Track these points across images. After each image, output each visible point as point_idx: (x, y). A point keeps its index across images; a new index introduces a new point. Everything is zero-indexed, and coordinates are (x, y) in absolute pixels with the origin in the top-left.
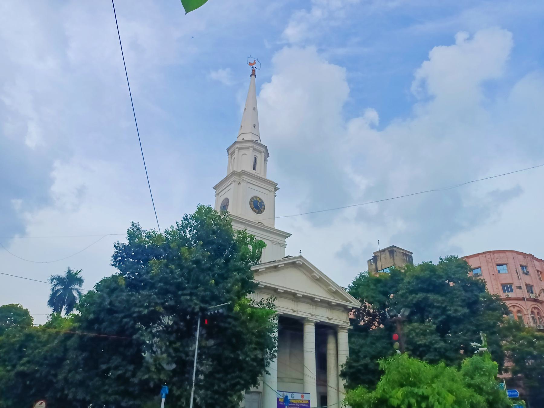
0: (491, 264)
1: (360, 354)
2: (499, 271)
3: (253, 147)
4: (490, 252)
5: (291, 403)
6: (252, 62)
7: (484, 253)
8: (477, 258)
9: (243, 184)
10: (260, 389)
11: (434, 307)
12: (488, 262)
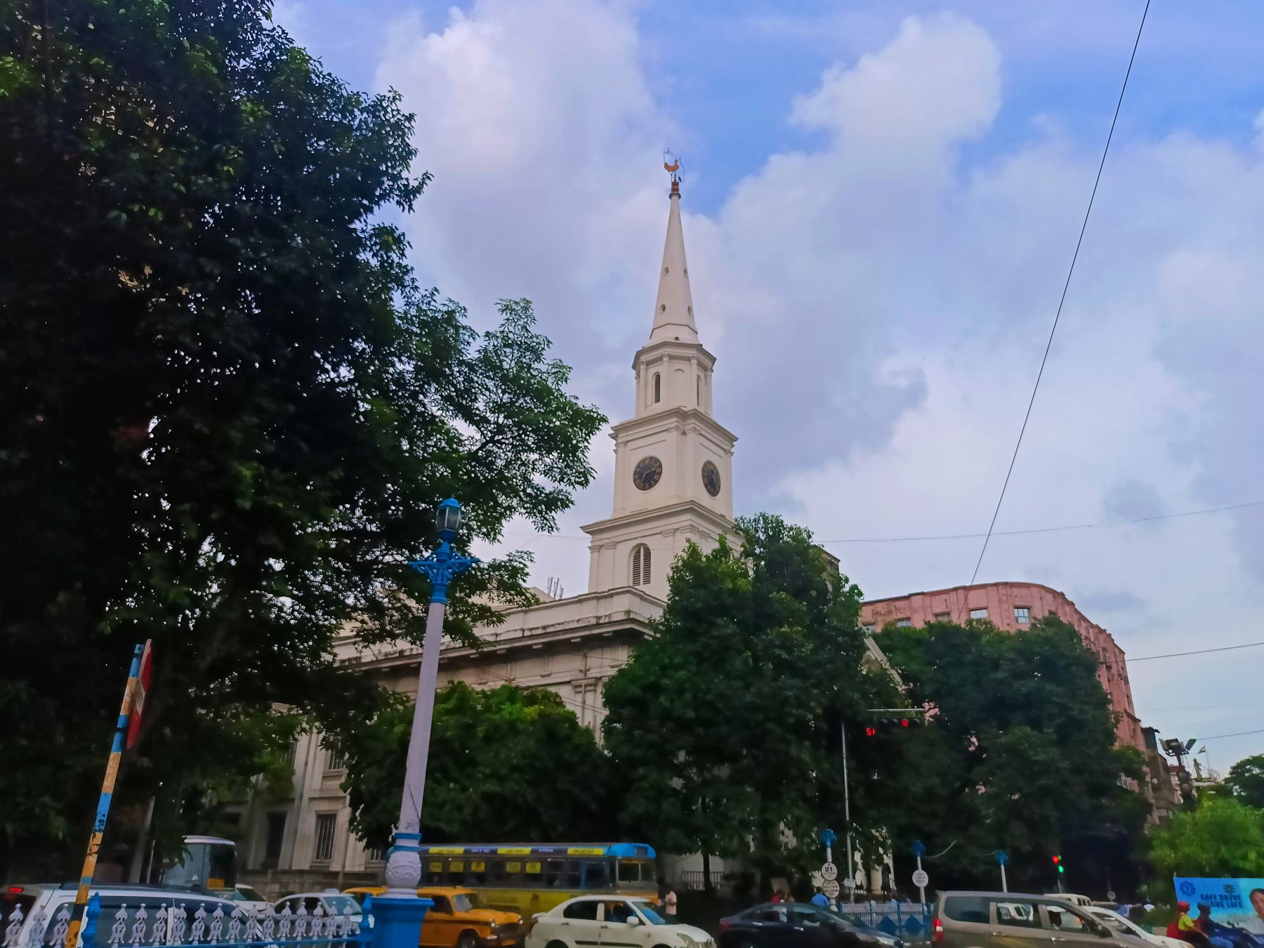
2: (1017, 619)
4: (1006, 584)
5: (158, 859)
6: (671, 164)
7: (996, 585)
8: (983, 591)
9: (691, 436)
10: (620, 883)
12: (1000, 601)
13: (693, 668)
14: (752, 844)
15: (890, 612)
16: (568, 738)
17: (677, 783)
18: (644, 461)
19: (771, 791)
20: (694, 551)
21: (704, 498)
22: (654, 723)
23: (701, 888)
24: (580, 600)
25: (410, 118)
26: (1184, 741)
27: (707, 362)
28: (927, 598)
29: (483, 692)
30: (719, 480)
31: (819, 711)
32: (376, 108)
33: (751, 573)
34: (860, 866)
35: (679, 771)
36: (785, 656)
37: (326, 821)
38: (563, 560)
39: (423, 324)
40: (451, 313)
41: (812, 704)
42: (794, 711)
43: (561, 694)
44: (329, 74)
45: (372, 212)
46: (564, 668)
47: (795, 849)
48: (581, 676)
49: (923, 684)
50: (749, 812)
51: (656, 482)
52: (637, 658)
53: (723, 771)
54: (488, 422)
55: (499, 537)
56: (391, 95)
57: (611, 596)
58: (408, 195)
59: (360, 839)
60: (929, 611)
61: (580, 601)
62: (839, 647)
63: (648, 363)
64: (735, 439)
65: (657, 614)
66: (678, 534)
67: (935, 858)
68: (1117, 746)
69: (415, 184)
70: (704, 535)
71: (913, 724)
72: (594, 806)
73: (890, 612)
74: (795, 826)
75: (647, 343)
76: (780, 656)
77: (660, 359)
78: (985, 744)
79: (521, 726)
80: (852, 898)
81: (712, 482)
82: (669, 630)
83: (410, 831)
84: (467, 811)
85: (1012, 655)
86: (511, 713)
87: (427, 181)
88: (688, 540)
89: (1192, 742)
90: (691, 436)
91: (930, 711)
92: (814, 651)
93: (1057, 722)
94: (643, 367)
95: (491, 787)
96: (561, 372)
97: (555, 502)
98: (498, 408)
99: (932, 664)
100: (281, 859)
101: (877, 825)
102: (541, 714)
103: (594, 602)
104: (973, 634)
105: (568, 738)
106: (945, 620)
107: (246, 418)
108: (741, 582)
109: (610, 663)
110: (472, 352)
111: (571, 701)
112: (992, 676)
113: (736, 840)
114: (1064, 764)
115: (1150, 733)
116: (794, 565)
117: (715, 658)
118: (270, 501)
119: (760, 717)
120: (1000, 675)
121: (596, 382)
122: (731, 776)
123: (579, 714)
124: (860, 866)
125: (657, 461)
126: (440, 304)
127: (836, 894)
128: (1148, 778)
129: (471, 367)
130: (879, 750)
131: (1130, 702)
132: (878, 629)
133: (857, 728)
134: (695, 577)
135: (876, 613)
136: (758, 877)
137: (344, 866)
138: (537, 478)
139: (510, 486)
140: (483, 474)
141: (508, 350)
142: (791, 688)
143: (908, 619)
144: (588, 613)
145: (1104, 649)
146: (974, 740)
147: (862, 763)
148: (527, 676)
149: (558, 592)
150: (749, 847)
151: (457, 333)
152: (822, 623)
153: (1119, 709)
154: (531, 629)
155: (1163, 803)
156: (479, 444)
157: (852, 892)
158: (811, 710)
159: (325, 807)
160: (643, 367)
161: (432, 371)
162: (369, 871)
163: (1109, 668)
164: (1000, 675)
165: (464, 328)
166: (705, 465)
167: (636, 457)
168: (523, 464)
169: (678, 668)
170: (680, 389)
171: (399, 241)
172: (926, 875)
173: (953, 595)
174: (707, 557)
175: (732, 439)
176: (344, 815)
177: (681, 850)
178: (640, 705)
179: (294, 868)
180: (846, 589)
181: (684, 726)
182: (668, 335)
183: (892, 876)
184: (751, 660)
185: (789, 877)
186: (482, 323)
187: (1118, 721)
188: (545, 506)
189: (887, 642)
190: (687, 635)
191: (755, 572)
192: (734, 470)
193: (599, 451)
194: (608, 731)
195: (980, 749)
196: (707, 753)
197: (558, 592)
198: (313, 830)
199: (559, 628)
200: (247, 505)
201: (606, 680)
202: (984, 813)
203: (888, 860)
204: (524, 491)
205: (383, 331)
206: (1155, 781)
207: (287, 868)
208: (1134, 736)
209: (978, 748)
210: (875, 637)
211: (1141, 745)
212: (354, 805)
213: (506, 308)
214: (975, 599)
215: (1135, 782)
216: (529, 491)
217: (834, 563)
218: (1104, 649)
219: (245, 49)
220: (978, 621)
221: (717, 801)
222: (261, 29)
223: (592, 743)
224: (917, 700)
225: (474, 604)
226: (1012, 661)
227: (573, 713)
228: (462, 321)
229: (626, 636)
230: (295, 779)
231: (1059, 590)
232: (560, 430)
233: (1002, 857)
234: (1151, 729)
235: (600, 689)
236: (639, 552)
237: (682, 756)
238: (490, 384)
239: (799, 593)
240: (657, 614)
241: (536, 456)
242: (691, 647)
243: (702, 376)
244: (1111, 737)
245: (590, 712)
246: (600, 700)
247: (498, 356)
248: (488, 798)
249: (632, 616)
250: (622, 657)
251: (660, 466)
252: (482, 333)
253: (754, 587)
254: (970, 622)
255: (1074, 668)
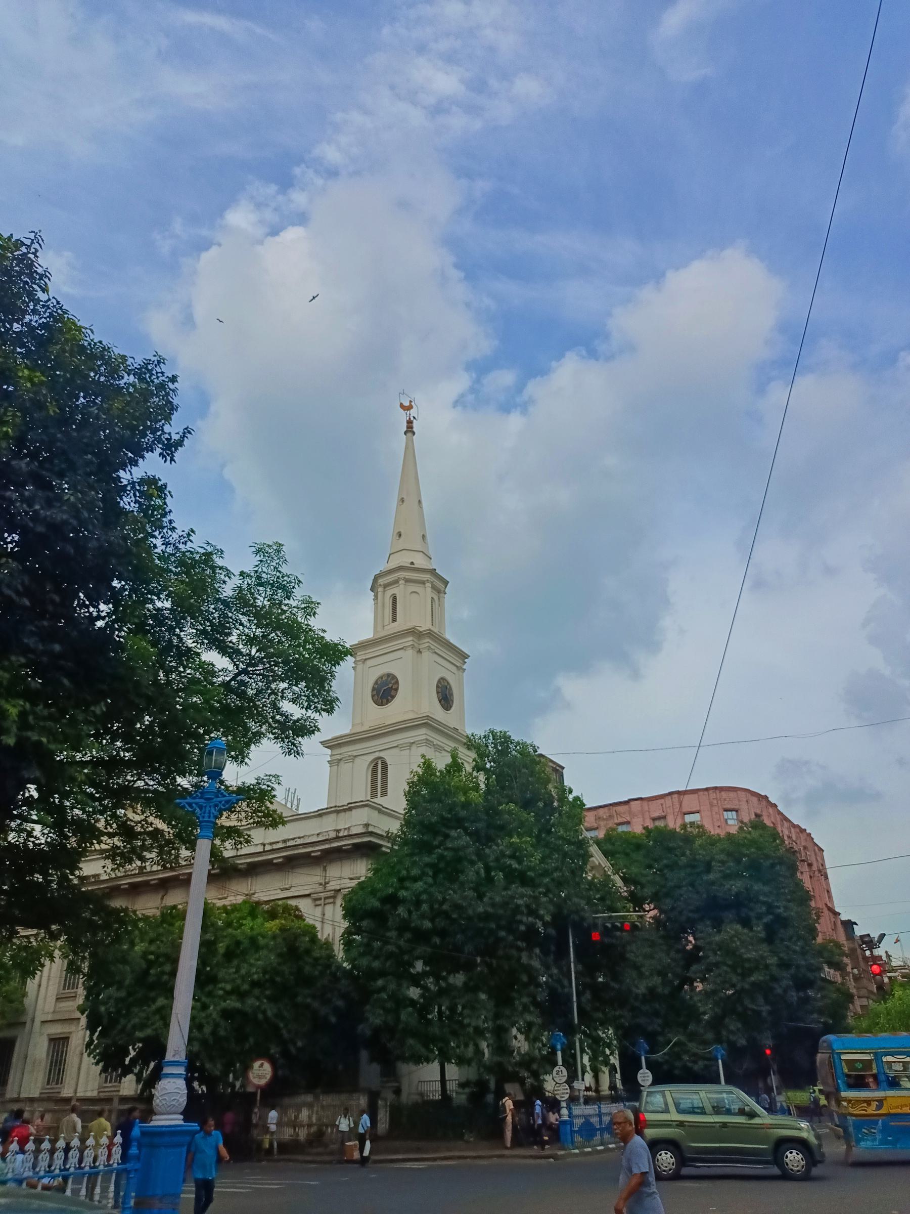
0: (716, 809)
1: (643, 970)
3: (432, 583)
4: (716, 788)
6: (407, 404)
7: (707, 789)
8: (696, 796)
9: (426, 654)
11: (758, 901)
12: (711, 805)
13: (430, 880)
14: (486, 1051)
15: (611, 817)
16: (308, 952)
17: (414, 993)
18: (381, 677)
19: (503, 999)
20: (428, 766)
21: (439, 714)
22: (393, 934)
23: (438, 1097)
24: (320, 814)
25: (173, 379)
26: (875, 935)
27: (440, 585)
28: (645, 803)
29: (224, 907)
30: (452, 695)
31: (548, 918)
32: (143, 372)
33: (483, 786)
34: (588, 1069)
35: (416, 981)
36: (515, 865)
37: (59, 1043)
38: (304, 779)
39: (181, 563)
40: (208, 555)
41: (542, 912)
42: (525, 919)
43: (301, 907)
44: (100, 342)
45: (136, 465)
46: (303, 882)
47: (527, 1054)
48: (321, 888)
49: (642, 888)
50: (483, 1019)
51: (393, 697)
52: (376, 871)
53: (458, 979)
54: (241, 653)
55: (246, 760)
56: (155, 359)
57: (350, 809)
58: (170, 448)
59: (97, 1064)
60: (647, 816)
61: (320, 815)
62: (565, 855)
63: (385, 586)
64: (467, 657)
65: (394, 827)
66: (414, 747)
67: (658, 1056)
68: (819, 940)
69: (177, 437)
70: (438, 749)
71: (634, 927)
72: (333, 1019)
73: (611, 817)
74: (527, 1030)
75: (383, 567)
76: (510, 865)
77: (396, 582)
78: (699, 943)
79: (262, 941)
80: (582, 1100)
81: (445, 697)
82: (405, 842)
83: (177, 1058)
84: (207, 1030)
85: (722, 857)
86: (252, 929)
87: (188, 435)
88: (423, 756)
89: (882, 936)
90: (426, 654)
91: (651, 913)
92: (542, 860)
93: (765, 920)
94: (380, 589)
95: (232, 1003)
96: (310, 608)
97: (303, 729)
98: (251, 641)
99: (650, 867)
100: (9, 1087)
101: (604, 1024)
102: (283, 929)
103: (333, 816)
104: (687, 838)
105: (308, 952)
106: (660, 824)
107: (13, 658)
108: (473, 795)
109: (352, 874)
110: (228, 591)
111: (310, 912)
112: (705, 878)
113: (471, 1048)
114: (772, 961)
115: (849, 925)
116: (522, 777)
117: (449, 870)
118: (34, 736)
119: (493, 926)
120: (711, 877)
121: (343, 616)
122: (465, 984)
123: (319, 928)
124: (588, 1069)
125: (394, 677)
126: (197, 544)
127: (567, 1096)
128: (849, 969)
129: (225, 603)
130: (603, 953)
131: (830, 897)
132: (601, 834)
133: (583, 931)
134: (429, 789)
135: (598, 818)
136: (492, 1085)
137: (76, 1092)
138: (287, 706)
139: (259, 714)
140: (233, 701)
141: (261, 588)
142: (522, 896)
143: (628, 823)
144: (328, 826)
145: (805, 848)
146: (691, 938)
147: (589, 968)
148: (267, 889)
149: (295, 803)
150: (483, 1054)
151: (214, 572)
152: (549, 832)
153: (821, 905)
154: (271, 844)
155: (864, 992)
156: (232, 675)
157: (582, 1094)
158: (541, 918)
159: (57, 1030)
160: (380, 589)
161: (185, 608)
162: (102, 1095)
163: (810, 865)
164: (711, 877)
165: (221, 568)
166: (439, 681)
167: (373, 674)
168: (274, 692)
169: (415, 879)
170: (415, 611)
171: (162, 489)
172: (650, 1074)
173: (668, 801)
174: (441, 771)
175: (464, 656)
176: (79, 1035)
177: (418, 1059)
178: (379, 917)
179: (23, 1095)
180: (571, 797)
181: (421, 936)
182: (404, 559)
183: (618, 1076)
184: (482, 871)
185: (522, 1082)
186: (237, 563)
187: (819, 917)
188: (292, 732)
189: (609, 847)
190: (424, 847)
191: (487, 785)
192: (467, 693)
193: (345, 678)
194: (348, 944)
195: (697, 948)
196: (441, 963)
197: (295, 803)
198: (44, 1055)
199: (299, 842)
200: (11, 741)
201: (345, 891)
202: (702, 1010)
203: (615, 1060)
204: (273, 718)
205: (143, 573)
206: (856, 971)
207: (16, 1096)
208: (835, 929)
209: (695, 946)
210: (598, 843)
211: (842, 938)
212: (91, 1027)
213: (258, 552)
214: (689, 803)
215: (838, 974)
216: (278, 717)
217: (558, 770)
218: (805, 848)
219: (16, 313)
220: (692, 824)
221: (453, 1009)
222: (39, 300)
223: (331, 956)
224: (637, 901)
225: (222, 827)
226: (723, 863)
227: (314, 927)
228: (219, 562)
229: (364, 849)
230: (27, 1001)
231: (763, 794)
232: (310, 664)
233: (720, 1052)
234: (849, 921)
235: (339, 901)
236: (376, 765)
237: (419, 966)
238: (244, 619)
239: (527, 805)
240: (394, 827)
241: (285, 685)
242: (427, 859)
243: (436, 598)
244: (813, 932)
245: (330, 925)
246: (340, 912)
247: (252, 594)
248: (227, 1014)
249: (371, 829)
250: (359, 870)
251: (397, 682)
252: (237, 573)
253: (486, 800)
254: (684, 826)
255: (778, 867)
